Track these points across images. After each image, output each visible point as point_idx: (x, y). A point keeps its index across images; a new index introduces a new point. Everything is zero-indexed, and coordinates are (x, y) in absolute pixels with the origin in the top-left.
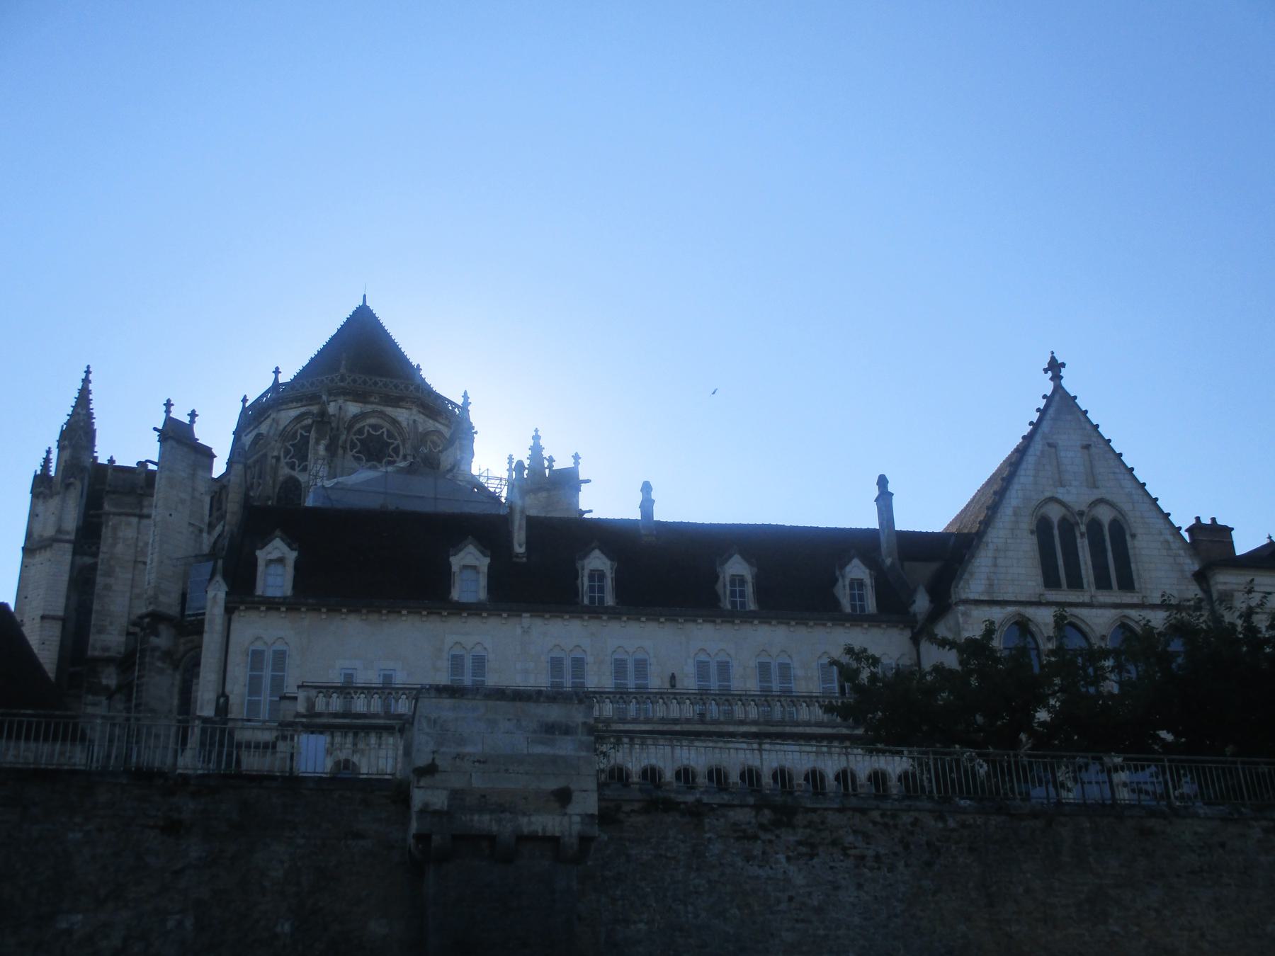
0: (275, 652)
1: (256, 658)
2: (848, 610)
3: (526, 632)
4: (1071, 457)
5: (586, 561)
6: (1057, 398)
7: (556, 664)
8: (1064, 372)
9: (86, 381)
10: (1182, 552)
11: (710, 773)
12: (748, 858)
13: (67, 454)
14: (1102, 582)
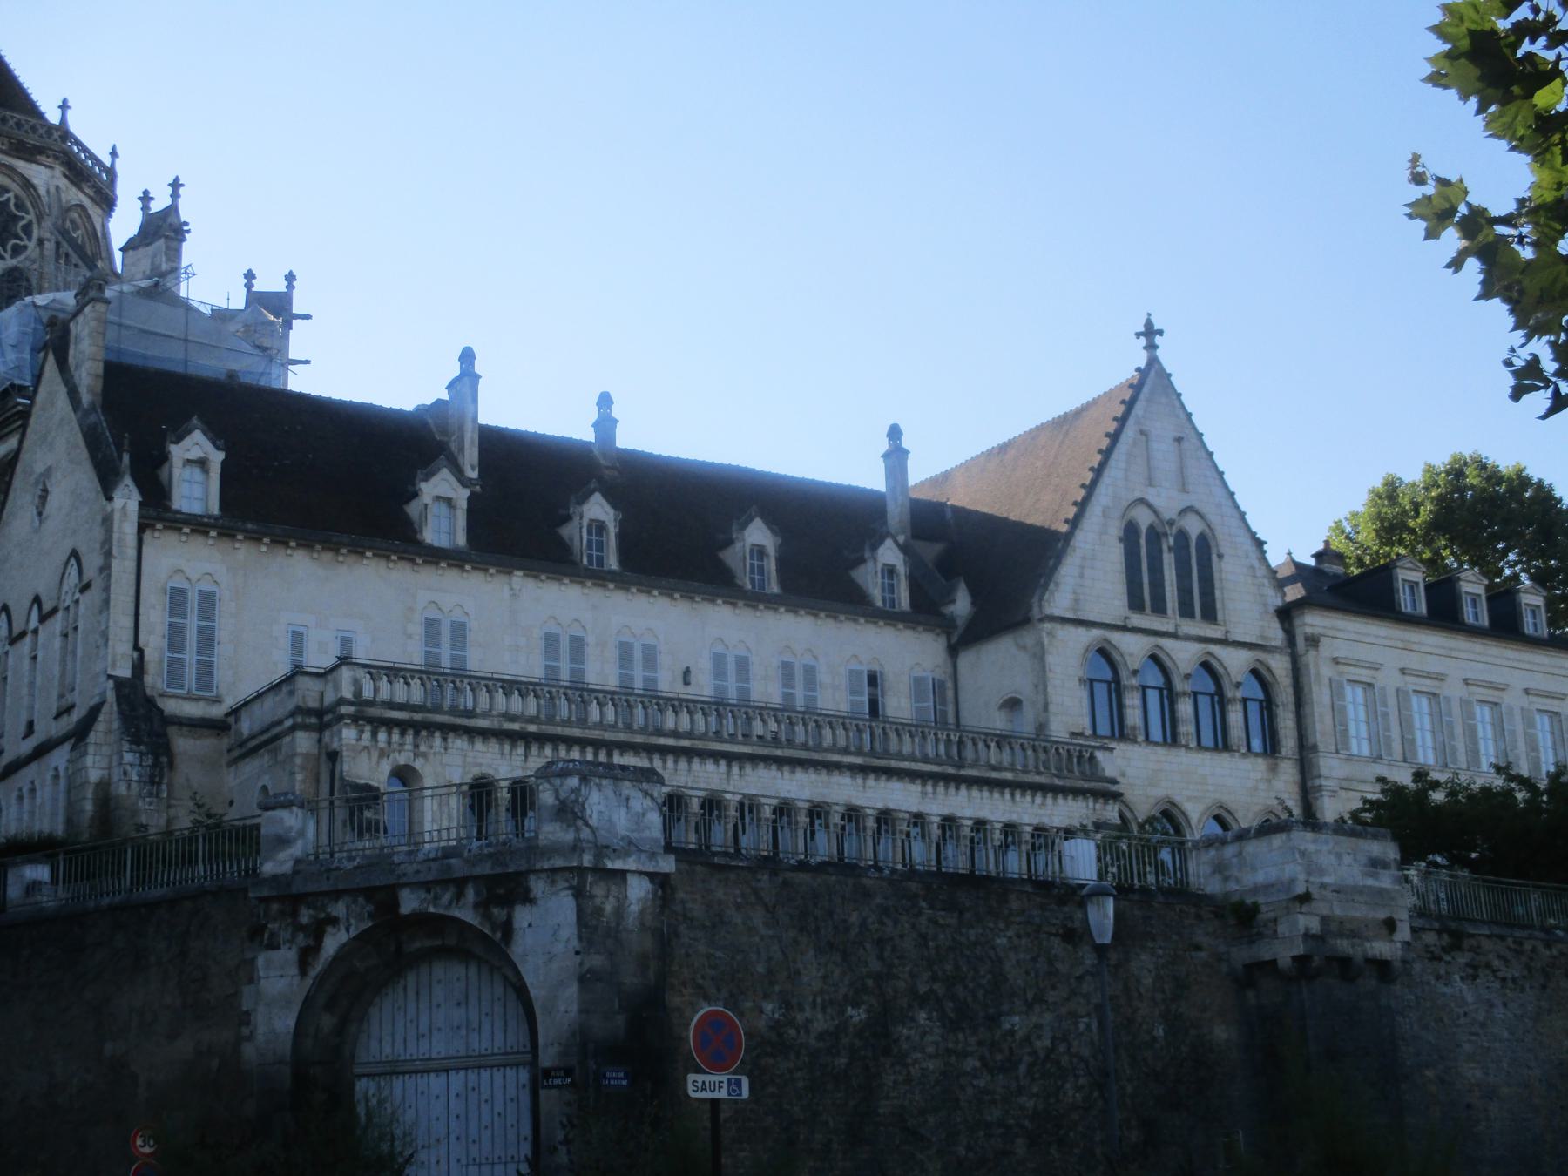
0: (201, 593)
1: (177, 599)
2: (879, 603)
3: (514, 596)
5: (585, 508)
6: (1153, 373)
7: (551, 641)
10: (1266, 582)
11: (741, 805)
12: (1438, 977)
14: (1186, 611)
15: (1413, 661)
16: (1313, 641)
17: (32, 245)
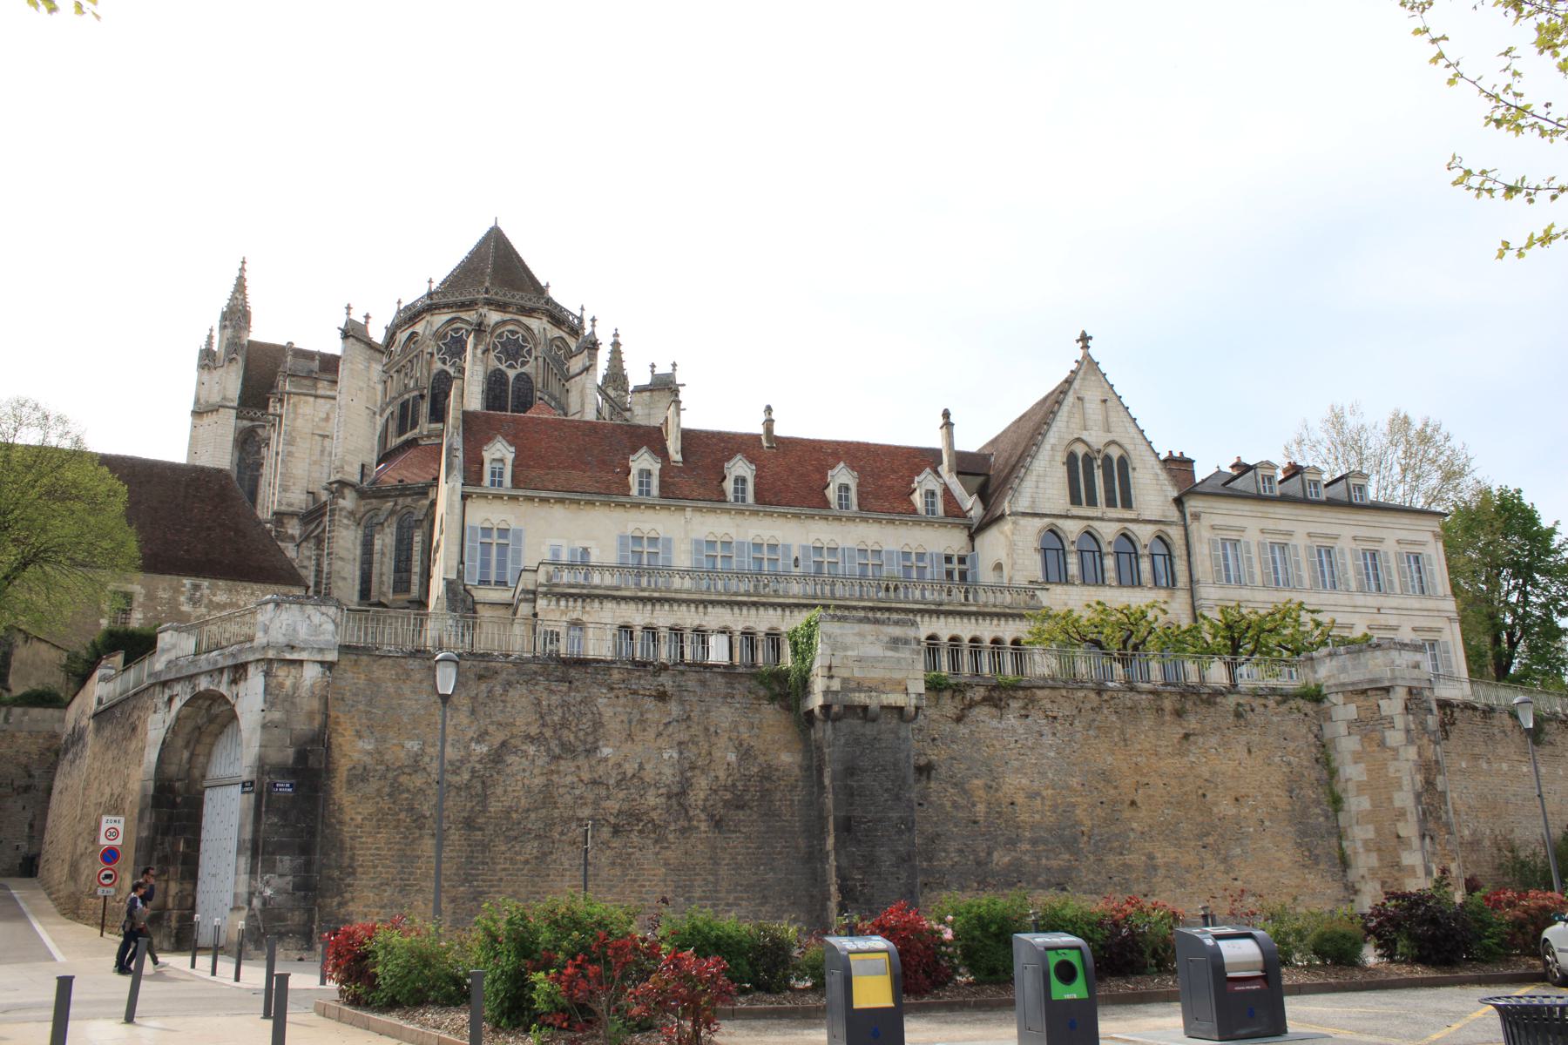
8: (1090, 343)
9: (242, 269)
13: (229, 332)
14: (1111, 502)
15: (1270, 525)
16: (1196, 516)
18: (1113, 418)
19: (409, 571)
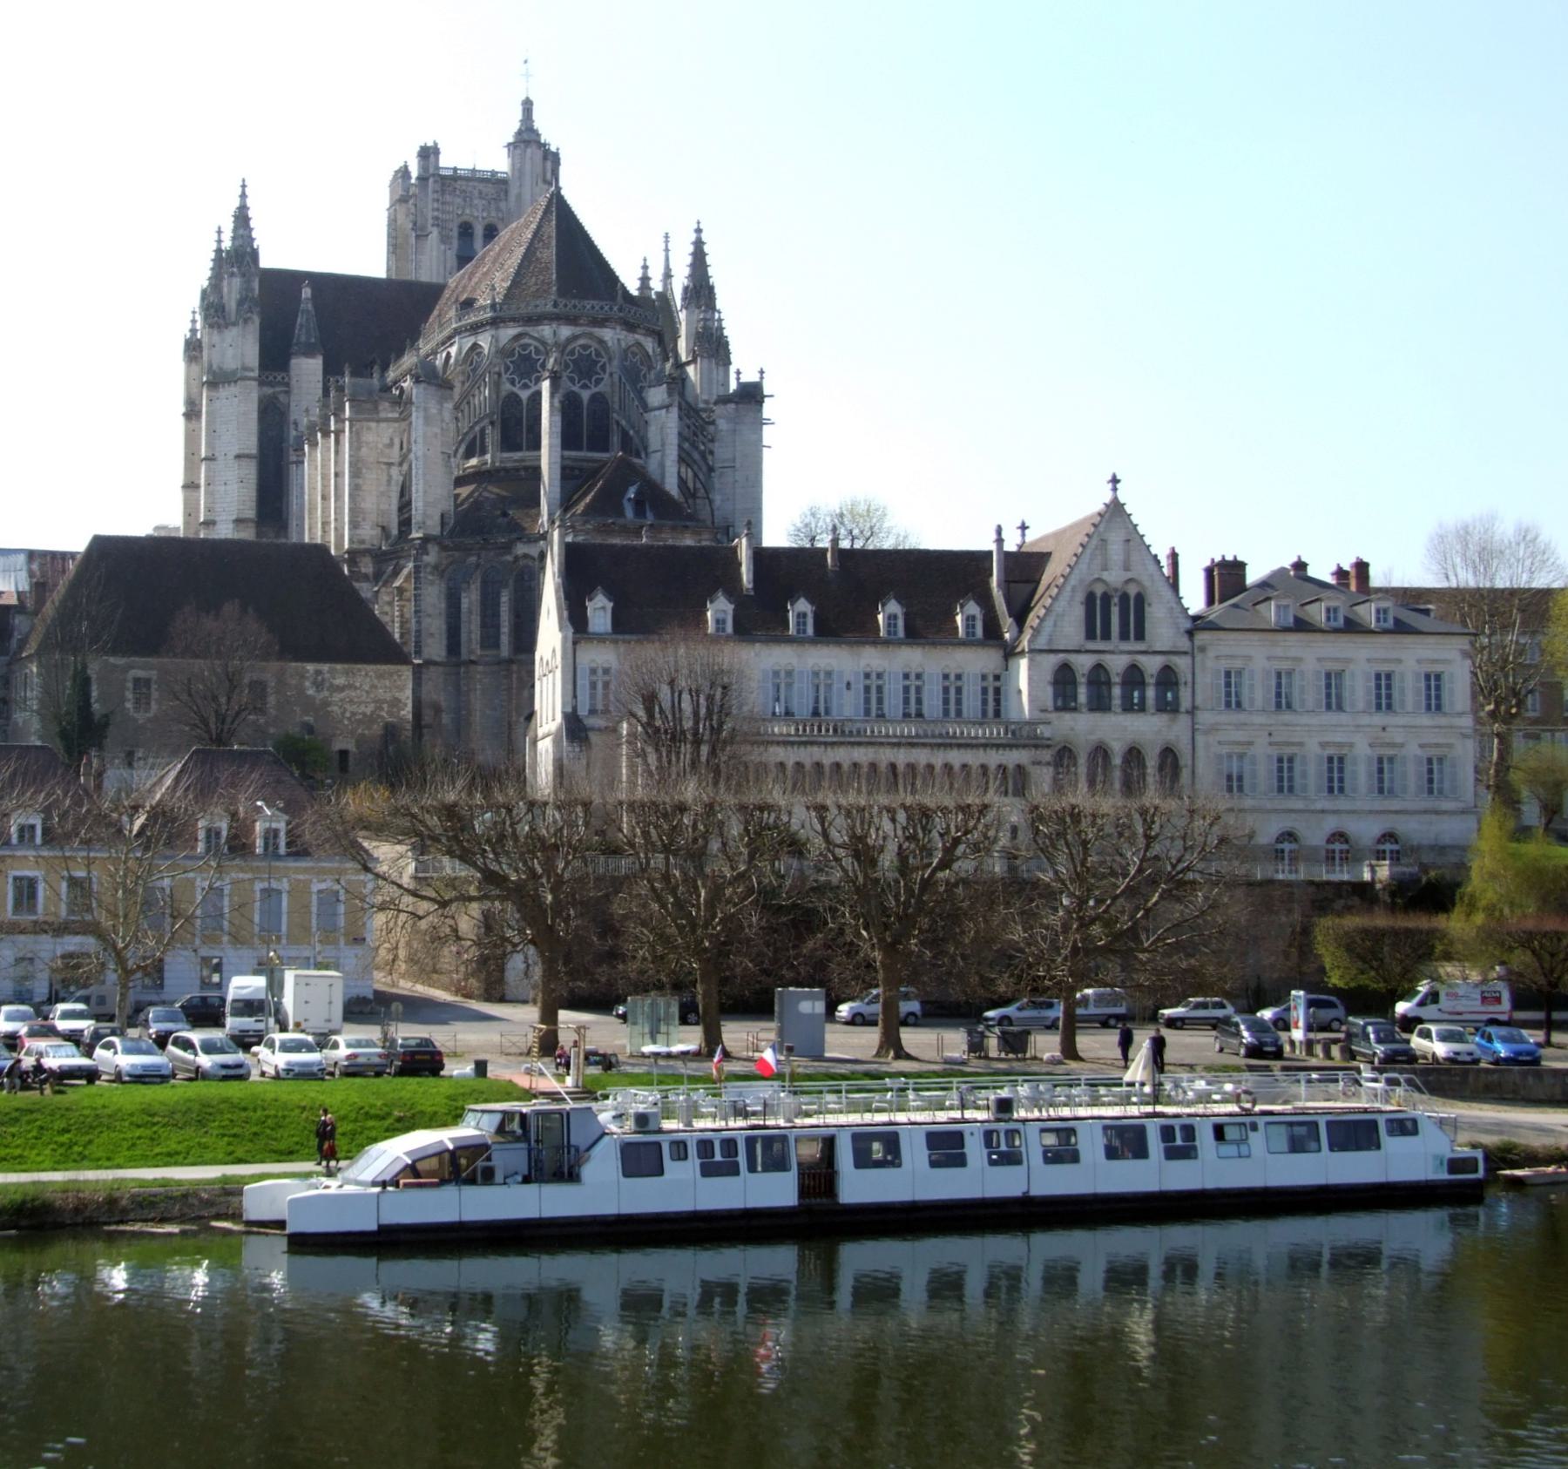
4: (1116, 550)
9: (243, 196)
14: (1124, 636)
15: (1279, 652)
16: (1203, 649)
17: (606, 376)
18: (1135, 557)
19: (498, 627)
